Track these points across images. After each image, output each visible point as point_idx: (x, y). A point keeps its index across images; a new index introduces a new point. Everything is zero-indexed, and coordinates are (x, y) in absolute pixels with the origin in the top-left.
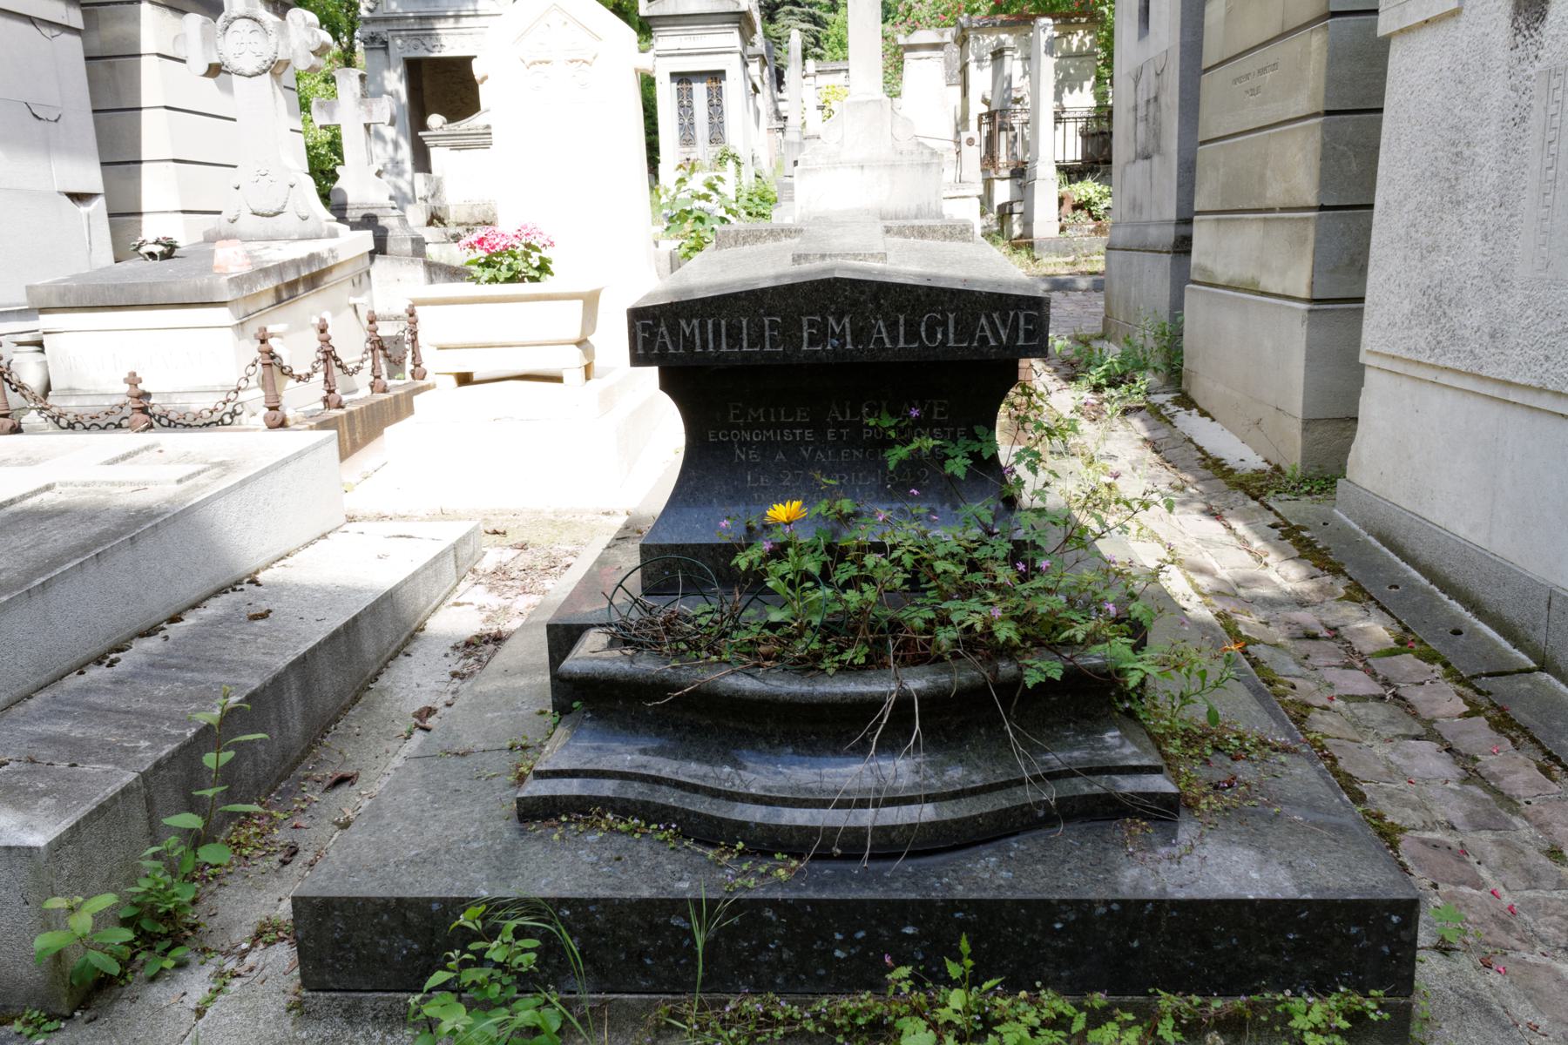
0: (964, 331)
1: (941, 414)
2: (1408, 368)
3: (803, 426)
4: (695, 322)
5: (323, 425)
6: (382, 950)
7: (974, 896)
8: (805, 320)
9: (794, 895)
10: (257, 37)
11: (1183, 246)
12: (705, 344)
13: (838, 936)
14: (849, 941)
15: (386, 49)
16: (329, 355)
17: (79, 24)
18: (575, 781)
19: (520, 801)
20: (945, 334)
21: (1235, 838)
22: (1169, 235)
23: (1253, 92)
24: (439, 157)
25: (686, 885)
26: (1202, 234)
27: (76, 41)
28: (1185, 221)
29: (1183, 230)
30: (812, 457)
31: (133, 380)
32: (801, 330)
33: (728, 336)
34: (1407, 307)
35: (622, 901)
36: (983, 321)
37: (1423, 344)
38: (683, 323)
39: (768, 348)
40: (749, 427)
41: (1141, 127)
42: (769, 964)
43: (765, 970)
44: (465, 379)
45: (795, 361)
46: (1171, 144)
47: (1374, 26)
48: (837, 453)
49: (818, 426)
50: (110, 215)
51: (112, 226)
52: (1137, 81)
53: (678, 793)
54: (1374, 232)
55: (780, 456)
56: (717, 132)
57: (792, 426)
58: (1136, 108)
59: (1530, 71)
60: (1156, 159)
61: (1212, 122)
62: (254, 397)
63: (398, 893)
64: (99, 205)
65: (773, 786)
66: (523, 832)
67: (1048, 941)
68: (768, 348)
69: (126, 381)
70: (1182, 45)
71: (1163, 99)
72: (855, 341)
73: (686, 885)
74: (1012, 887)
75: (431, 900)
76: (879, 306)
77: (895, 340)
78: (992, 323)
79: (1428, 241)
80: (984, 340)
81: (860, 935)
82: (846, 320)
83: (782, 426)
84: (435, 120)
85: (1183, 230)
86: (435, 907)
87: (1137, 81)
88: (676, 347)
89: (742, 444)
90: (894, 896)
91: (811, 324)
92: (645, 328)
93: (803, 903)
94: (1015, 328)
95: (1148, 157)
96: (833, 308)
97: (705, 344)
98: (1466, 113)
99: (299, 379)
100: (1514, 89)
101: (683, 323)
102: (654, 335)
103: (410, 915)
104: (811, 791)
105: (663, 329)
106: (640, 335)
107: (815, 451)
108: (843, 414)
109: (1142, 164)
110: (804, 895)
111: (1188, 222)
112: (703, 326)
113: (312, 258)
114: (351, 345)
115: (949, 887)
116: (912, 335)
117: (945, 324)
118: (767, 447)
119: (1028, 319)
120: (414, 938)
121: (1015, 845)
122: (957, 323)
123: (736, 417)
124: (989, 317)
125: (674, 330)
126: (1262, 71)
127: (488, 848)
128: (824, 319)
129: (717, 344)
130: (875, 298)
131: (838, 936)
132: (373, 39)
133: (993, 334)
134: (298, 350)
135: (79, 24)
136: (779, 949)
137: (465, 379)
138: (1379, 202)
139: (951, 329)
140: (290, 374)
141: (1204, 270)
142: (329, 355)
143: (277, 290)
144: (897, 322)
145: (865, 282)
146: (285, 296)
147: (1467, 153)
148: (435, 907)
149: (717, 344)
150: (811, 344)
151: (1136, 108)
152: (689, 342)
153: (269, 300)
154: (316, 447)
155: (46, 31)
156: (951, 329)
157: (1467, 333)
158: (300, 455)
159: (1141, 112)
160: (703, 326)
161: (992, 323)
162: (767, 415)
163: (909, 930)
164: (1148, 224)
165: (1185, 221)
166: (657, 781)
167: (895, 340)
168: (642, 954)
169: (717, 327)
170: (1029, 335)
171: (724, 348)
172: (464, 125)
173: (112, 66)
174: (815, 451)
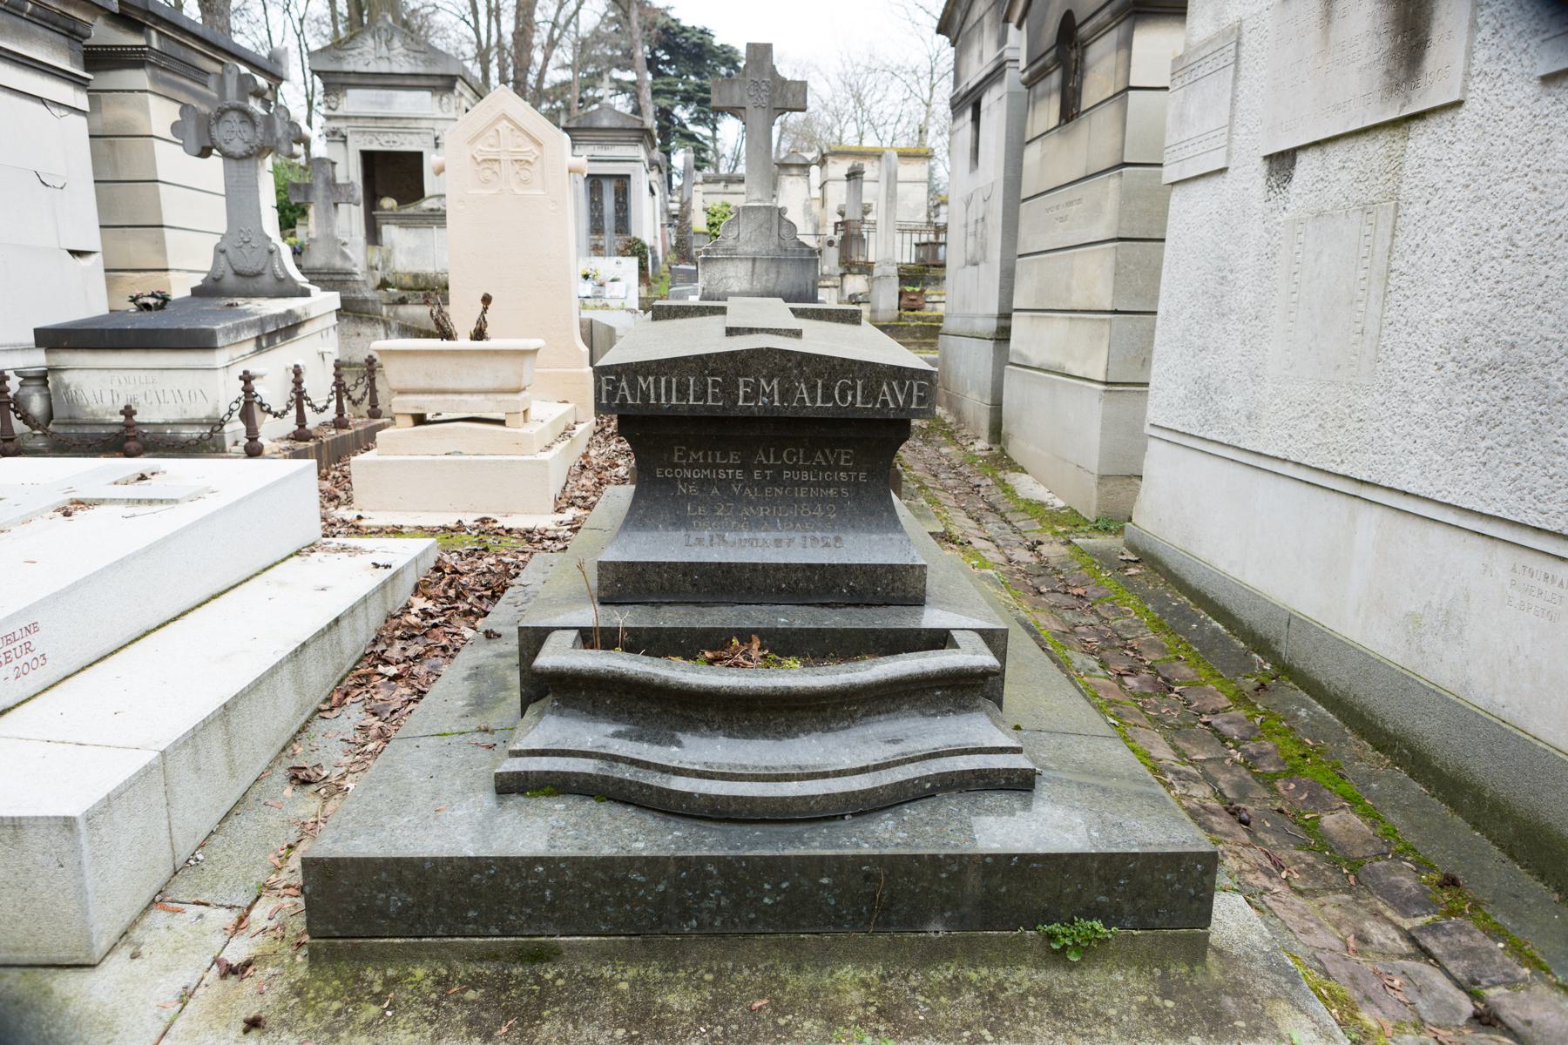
0: (870, 395)
1: (847, 461)
2: (1183, 439)
3: (733, 466)
4: (651, 379)
5: (296, 455)
6: (379, 903)
7: (876, 852)
8: (741, 380)
9: (732, 853)
10: (247, 128)
11: (1003, 335)
12: (658, 397)
13: (767, 886)
14: (776, 888)
15: (345, 142)
16: (299, 396)
17: (85, 106)
18: (545, 759)
19: (497, 776)
20: (854, 397)
21: (1077, 804)
22: (993, 324)
23: (1062, 219)
24: (390, 232)
25: (641, 845)
26: (1018, 324)
27: (83, 120)
28: (1005, 316)
29: (1003, 323)
30: (741, 493)
31: (128, 412)
32: (737, 388)
33: (678, 391)
34: (1182, 392)
35: (588, 858)
36: (885, 387)
37: (1194, 421)
38: (641, 379)
39: (710, 403)
40: (690, 466)
41: (971, 240)
42: (710, 910)
43: (706, 916)
44: (420, 420)
45: (732, 414)
46: (995, 255)
47: (1160, 175)
48: (762, 490)
49: (746, 467)
50: (107, 271)
51: (108, 279)
52: (968, 204)
53: (633, 769)
54: (1157, 333)
55: (715, 491)
56: (623, 224)
57: (726, 467)
58: (966, 226)
59: (1280, 219)
60: (982, 266)
61: (1029, 239)
62: (235, 429)
63: (395, 854)
64: (95, 263)
65: (704, 759)
66: (500, 804)
67: (935, 887)
68: (710, 403)
69: (122, 413)
70: (1006, 179)
71: (989, 219)
72: (782, 400)
73: (641, 845)
74: (907, 844)
75: (424, 859)
76: (802, 373)
77: (814, 400)
78: (892, 389)
79: (1199, 342)
80: (885, 403)
81: (784, 885)
82: (775, 382)
83: (718, 466)
84: (388, 203)
85: (1003, 323)
86: (428, 865)
87: (968, 204)
88: (634, 399)
89: (685, 480)
90: (812, 852)
91: (746, 385)
92: (609, 382)
93: (740, 859)
94: (910, 395)
95: (976, 264)
96: (765, 372)
97: (658, 397)
98: (1230, 247)
99: (276, 415)
100: (1267, 231)
101: (641, 379)
102: (616, 388)
103: (406, 872)
104: (745, 767)
105: (624, 384)
106: (604, 388)
107: (743, 488)
108: (768, 459)
109: (970, 269)
110: (740, 853)
111: (1008, 317)
112: (657, 382)
113: (290, 312)
114: (319, 385)
115: (858, 846)
116: (828, 397)
117: (854, 388)
118: (704, 483)
119: (920, 388)
120: (409, 892)
121: (909, 812)
122: (864, 388)
123: (680, 458)
124: (889, 385)
125: (633, 385)
126: (1070, 204)
127: (471, 816)
128: (757, 380)
129: (669, 398)
130: (799, 365)
131: (767, 886)
132: (334, 133)
133: (892, 398)
134: (273, 390)
135: (85, 106)
136: (718, 898)
137: (420, 420)
138: (1161, 310)
139: (859, 393)
140: (269, 411)
141: (1020, 355)
142: (299, 396)
143: (258, 339)
144: (816, 386)
145: (792, 352)
146: (264, 344)
147: (1230, 277)
148: (428, 865)
149: (669, 398)
150: (745, 400)
151: (966, 226)
152: (645, 396)
153: (251, 347)
154: (298, 474)
155: (56, 111)
156: (859, 393)
157: (1228, 414)
158: (285, 480)
159: (971, 229)
160: (657, 382)
161: (892, 389)
162: (705, 457)
163: (825, 881)
164: (974, 317)
165: (1005, 316)
166: (615, 759)
167: (814, 400)
168: (604, 902)
169: (669, 383)
170: (921, 400)
171: (674, 402)
172: (410, 210)
173: (112, 144)
174: (743, 488)
